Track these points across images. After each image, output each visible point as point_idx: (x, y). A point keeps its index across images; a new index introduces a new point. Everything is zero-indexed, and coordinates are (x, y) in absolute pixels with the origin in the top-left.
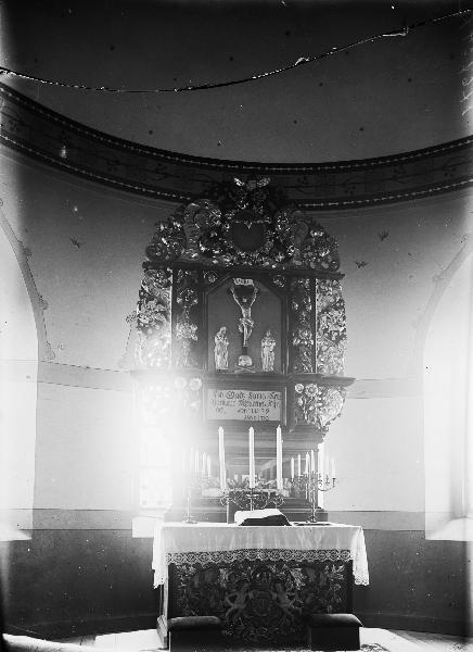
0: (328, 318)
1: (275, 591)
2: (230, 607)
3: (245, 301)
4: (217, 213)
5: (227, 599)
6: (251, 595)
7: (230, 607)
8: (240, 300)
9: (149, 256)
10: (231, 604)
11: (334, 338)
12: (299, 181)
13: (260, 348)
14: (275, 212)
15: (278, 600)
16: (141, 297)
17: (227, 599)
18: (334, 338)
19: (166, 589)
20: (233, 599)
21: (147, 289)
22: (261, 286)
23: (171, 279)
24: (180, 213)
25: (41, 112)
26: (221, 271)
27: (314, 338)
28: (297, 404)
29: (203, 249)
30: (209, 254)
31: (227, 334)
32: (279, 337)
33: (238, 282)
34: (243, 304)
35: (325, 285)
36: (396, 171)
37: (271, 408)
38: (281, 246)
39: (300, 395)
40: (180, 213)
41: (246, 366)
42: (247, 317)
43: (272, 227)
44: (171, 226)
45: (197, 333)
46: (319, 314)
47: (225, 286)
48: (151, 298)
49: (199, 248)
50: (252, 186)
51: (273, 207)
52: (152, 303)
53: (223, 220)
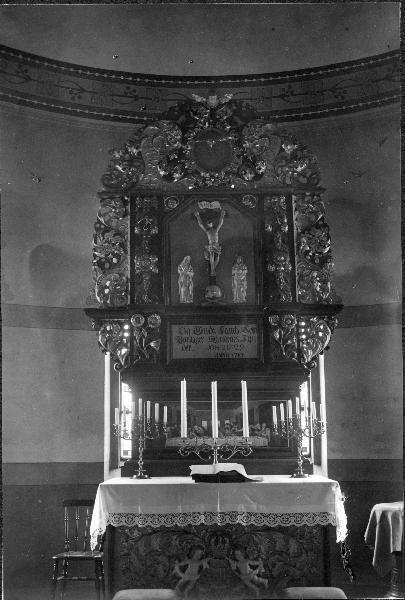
0: (309, 239)
1: (235, 560)
2: (181, 578)
3: (211, 225)
4: (177, 134)
5: (177, 568)
6: (205, 565)
7: (181, 578)
8: (205, 226)
9: (106, 185)
10: (180, 574)
11: (317, 261)
12: (389, 70)
13: (231, 276)
14: (242, 127)
15: (238, 570)
16: (97, 229)
17: (177, 568)
18: (317, 261)
19: (402, 514)
20: (183, 569)
21: (102, 220)
22: (229, 209)
23: (129, 207)
24: (137, 137)
25: (37, 62)
26: (185, 198)
27: (292, 262)
28: (274, 338)
29: (162, 173)
30: (169, 178)
31: (192, 263)
32: (252, 267)
33: (203, 205)
34: (208, 229)
35: (303, 202)
36: (80, 97)
37: (246, 343)
38: (250, 163)
39: (276, 328)
40: (137, 137)
41: (214, 298)
42: (214, 243)
43: (239, 143)
44: (127, 152)
45: (158, 265)
46: (299, 234)
47: (189, 212)
48: (107, 230)
49: (158, 173)
50: (213, 101)
51: (240, 123)
52: (109, 236)
53: (184, 141)
